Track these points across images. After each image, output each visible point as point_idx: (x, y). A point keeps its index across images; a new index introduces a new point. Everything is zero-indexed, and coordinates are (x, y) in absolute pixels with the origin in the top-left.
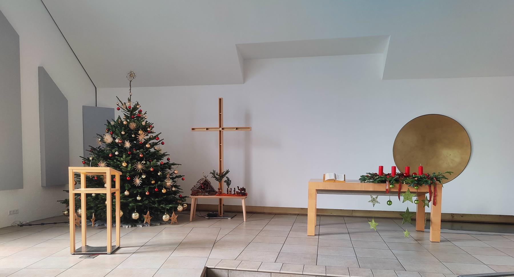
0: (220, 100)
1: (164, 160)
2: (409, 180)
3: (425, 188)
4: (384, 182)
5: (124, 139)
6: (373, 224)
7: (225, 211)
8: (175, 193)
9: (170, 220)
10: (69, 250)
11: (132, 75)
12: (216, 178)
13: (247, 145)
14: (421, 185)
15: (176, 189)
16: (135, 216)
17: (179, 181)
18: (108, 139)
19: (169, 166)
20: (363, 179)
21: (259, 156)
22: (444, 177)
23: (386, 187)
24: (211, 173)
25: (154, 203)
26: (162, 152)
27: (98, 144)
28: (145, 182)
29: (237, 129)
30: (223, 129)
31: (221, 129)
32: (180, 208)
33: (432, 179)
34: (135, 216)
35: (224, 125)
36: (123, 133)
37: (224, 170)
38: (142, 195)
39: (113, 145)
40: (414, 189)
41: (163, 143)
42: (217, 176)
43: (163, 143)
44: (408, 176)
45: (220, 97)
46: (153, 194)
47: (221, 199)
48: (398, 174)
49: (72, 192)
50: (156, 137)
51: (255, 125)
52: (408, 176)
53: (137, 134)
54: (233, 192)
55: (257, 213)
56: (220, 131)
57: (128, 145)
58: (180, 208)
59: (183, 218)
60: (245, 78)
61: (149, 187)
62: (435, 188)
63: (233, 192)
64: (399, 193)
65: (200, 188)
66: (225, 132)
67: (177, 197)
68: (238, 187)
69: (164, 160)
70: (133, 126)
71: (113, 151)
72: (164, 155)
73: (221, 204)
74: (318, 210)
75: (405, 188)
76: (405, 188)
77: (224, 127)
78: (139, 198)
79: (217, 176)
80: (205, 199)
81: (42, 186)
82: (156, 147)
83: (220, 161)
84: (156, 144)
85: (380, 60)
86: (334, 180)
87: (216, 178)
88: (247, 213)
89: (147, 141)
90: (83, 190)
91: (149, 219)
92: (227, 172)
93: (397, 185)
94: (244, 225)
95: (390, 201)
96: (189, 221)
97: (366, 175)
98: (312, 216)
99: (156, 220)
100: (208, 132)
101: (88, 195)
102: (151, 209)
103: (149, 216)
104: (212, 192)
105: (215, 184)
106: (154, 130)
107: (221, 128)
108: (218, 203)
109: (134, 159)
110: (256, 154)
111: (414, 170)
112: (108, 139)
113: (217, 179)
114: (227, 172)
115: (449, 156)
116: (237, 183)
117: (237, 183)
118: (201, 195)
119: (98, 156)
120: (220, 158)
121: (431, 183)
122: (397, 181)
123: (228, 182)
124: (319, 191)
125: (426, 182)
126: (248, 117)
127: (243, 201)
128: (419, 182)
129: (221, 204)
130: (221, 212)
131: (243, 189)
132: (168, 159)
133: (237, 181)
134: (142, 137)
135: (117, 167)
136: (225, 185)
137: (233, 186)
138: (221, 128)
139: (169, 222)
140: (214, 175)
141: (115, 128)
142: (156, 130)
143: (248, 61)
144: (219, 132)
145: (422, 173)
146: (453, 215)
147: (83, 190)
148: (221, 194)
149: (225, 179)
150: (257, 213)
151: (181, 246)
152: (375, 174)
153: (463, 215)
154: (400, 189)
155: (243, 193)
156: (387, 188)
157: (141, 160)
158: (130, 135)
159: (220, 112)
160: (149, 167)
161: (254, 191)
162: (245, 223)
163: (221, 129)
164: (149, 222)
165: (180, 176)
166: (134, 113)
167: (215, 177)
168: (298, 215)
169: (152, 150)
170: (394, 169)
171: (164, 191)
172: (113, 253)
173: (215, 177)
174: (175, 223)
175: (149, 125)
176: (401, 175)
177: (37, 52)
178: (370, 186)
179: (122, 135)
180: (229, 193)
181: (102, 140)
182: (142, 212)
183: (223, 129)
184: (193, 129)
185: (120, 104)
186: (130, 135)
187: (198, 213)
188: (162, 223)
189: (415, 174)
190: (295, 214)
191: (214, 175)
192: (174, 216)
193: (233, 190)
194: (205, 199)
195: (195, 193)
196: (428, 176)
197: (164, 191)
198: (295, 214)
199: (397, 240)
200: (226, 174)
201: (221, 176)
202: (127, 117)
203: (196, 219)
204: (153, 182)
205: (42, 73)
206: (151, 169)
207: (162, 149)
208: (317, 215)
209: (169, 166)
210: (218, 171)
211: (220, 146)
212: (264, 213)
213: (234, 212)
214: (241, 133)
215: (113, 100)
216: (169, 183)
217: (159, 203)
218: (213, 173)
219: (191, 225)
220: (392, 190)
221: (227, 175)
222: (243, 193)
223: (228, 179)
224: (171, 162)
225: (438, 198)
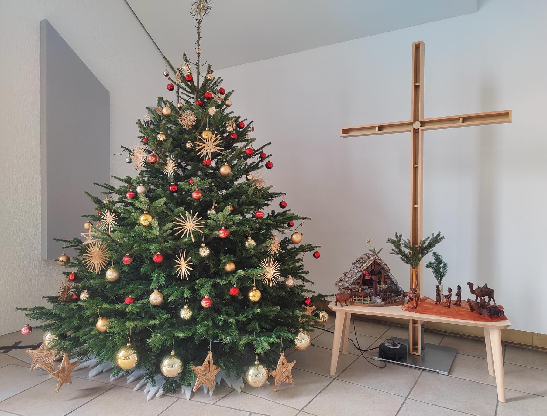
6: (419, 165)
12: (404, 255)
15: (299, 282)
16: (171, 366)
19: (284, 220)
24: (390, 241)
28: (201, 269)
31: (417, 125)
34: (171, 366)
35: (427, 114)
37: (426, 233)
42: (407, 251)
43: (269, 166)
56: (416, 131)
58: (302, 340)
60: (479, 8)
61: (215, 285)
65: (364, 281)
68: (471, 285)
69: (273, 207)
79: (407, 251)
82: (252, 175)
83: (415, 210)
84: (254, 167)
87: (404, 255)
92: (437, 240)
103: (213, 366)
104: (392, 295)
105: (400, 273)
106: (250, 135)
113: (407, 259)
114: (437, 240)
120: (415, 202)
123: (439, 269)
130: (415, 343)
136: (428, 279)
137: (450, 281)
140: (398, 247)
144: (410, 135)
149: (428, 258)
163: (417, 125)
165: (310, 248)
167: (401, 252)
183: (423, 124)
184: (345, 131)
191: (398, 247)
193: (455, 291)
204: (230, 267)
206: (222, 234)
207: (263, 178)
210: (408, 236)
211: (415, 169)
214: (472, 131)
218: (396, 243)
221: (436, 249)
223: (439, 260)
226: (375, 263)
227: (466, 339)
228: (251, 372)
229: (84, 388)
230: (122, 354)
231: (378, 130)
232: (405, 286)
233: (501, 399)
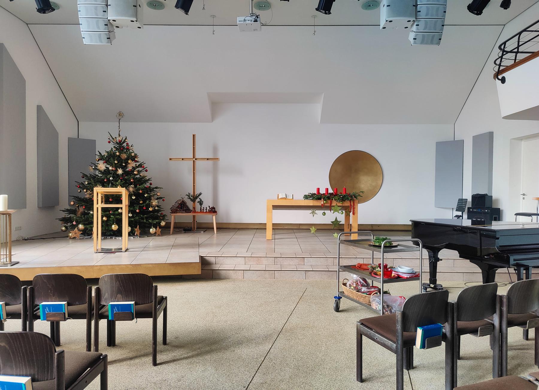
0: (194, 135)
1: (148, 185)
2: (337, 197)
3: (347, 204)
4: (319, 199)
7: (197, 228)
8: (158, 211)
9: (155, 233)
10: (93, 250)
13: (215, 172)
14: (344, 201)
18: (102, 166)
20: (306, 197)
21: (226, 183)
22: (359, 195)
23: (321, 203)
24: (187, 195)
25: (143, 219)
26: (147, 178)
27: (90, 171)
29: (208, 159)
30: (196, 159)
31: (194, 159)
32: (163, 223)
33: (351, 197)
36: (116, 162)
37: (197, 193)
39: (106, 172)
41: (146, 171)
43: (146, 171)
44: (336, 195)
46: (143, 212)
47: (194, 216)
48: (330, 194)
50: (140, 166)
51: (221, 156)
52: (336, 195)
53: (127, 163)
54: (205, 211)
55: (224, 228)
56: (194, 161)
57: (120, 172)
58: (163, 223)
59: (165, 231)
60: (213, 119)
62: (354, 203)
63: (205, 211)
64: (330, 208)
65: (178, 207)
66: (197, 162)
67: (159, 214)
69: (148, 185)
70: (124, 156)
71: (108, 176)
72: (149, 180)
73: (194, 221)
74: (273, 224)
75: (334, 203)
76: (334, 203)
77: (197, 157)
80: (185, 218)
81: (38, 207)
83: (194, 185)
84: (141, 171)
85: (317, 109)
86: (286, 198)
88: (217, 228)
89: (134, 168)
91: (139, 232)
92: (200, 194)
93: (329, 201)
94: (215, 235)
95: (324, 213)
96: (168, 234)
97: (308, 194)
98: (269, 228)
99: (145, 233)
100: (183, 161)
104: (188, 210)
105: (190, 204)
107: (195, 159)
108: (191, 220)
110: (224, 181)
111: (340, 191)
112: (102, 166)
113: (192, 200)
115: (365, 182)
116: (208, 203)
117: (208, 203)
118: (180, 213)
120: (194, 183)
121: (351, 200)
122: (329, 198)
123: (201, 203)
124: (275, 207)
125: (348, 198)
126: (215, 150)
127: (214, 217)
128: (343, 199)
129: (194, 221)
131: (213, 208)
132: (151, 184)
134: (131, 165)
137: (205, 205)
138: (195, 159)
139: (155, 234)
141: (109, 158)
142: (140, 159)
143: (217, 105)
145: (346, 193)
146: (372, 225)
148: (195, 212)
149: (198, 200)
150: (224, 228)
151: (174, 246)
152: (315, 194)
153: (379, 225)
154: (331, 204)
155: (213, 210)
156: (322, 203)
159: (194, 145)
160: (139, 189)
161: (221, 209)
162: (215, 235)
163: (194, 159)
164: (138, 234)
165: (161, 198)
166: (122, 146)
167: (190, 198)
168: (257, 229)
169: (138, 176)
170: (327, 190)
171: (150, 209)
172: (126, 251)
173: (190, 198)
174: (159, 235)
176: (331, 194)
177: (39, 92)
178: (311, 203)
179: (116, 164)
180: (201, 211)
181: (96, 169)
183: (196, 159)
184: (170, 159)
185: (111, 138)
187: (175, 230)
188: (149, 234)
189: (341, 193)
190: (255, 229)
192: (159, 230)
193: (205, 209)
194: (185, 218)
195: (174, 211)
196: (349, 195)
197: (150, 209)
198: (255, 229)
199: (328, 241)
200: (199, 196)
201: (194, 198)
203: (175, 233)
204: (141, 202)
205: (40, 109)
206: (141, 192)
207: (147, 175)
208: (273, 229)
210: (192, 193)
211: (194, 173)
212: (229, 229)
213: (206, 228)
214: (210, 162)
216: (155, 203)
219: (171, 236)
220: (326, 205)
222: (213, 210)
223: (201, 200)
224: (152, 186)
225: (355, 210)
226: (183, 201)
227: (239, 229)
228: (151, 230)
229: (38, 383)
230: (113, 226)
231: (102, 208)
232: (191, 208)
233: (196, 227)
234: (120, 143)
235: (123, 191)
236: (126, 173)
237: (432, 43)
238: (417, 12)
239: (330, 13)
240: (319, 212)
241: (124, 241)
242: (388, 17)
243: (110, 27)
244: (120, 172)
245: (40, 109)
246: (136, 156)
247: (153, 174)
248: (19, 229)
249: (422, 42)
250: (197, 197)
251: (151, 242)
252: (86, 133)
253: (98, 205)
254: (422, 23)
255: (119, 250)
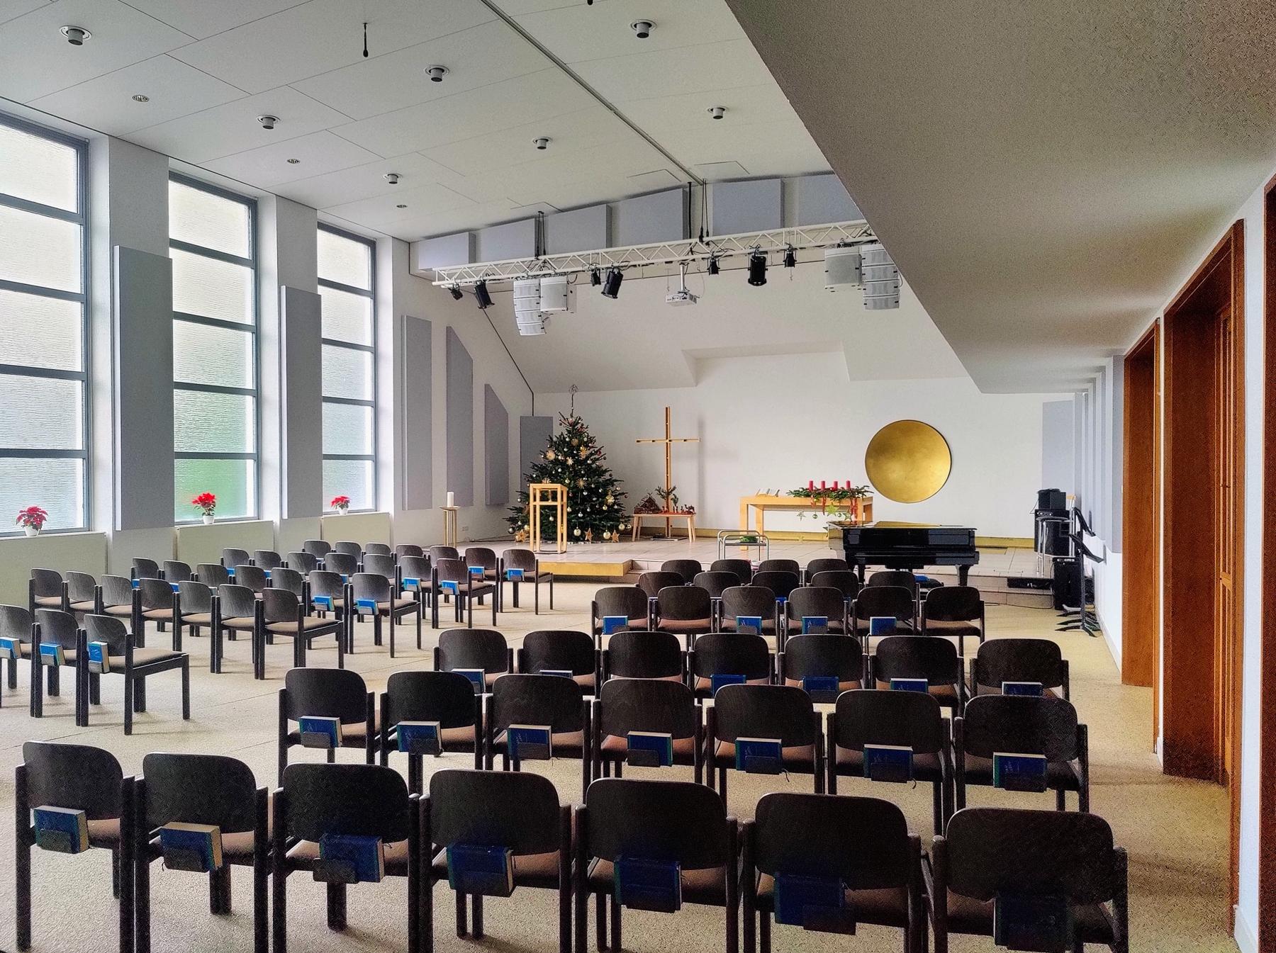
1: (607, 476)
3: (846, 502)
4: (808, 496)
5: (566, 455)
8: (617, 511)
11: (714, 269)
16: (577, 532)
17: (622, 499)
18: (551, 455)
19: (611, 482)
20: (797, 494)
23: (808, 501)
27: (540, 460)
34: (577, 532)
38: (584, 512)
40: (836, 503)
45: (609, 299)
49: (532, 503)
53: (578, 450)
58: (622, 527)
59: (626, 536)
60: (697, 384)
64: (823, 508)
65: (644, 506)
69: (607, 476)
70: (575, 442)
72: (606, 471)
75: (829, 502)
78: (580, 515)
80: (650, 520)
89: (587, 458)
90: (538, 503)
99: (598, 538)
101: (542, 507)
102: (593, 526)
104: (656, 510)
105: (660, 502)
109: (576, 475)
110: (711, 467)
112: (551, 455)
119: (544, 472)
126: (701, 426)
133: (687, 496)
134: (584, 453)
135: (562, 483)
136: (671, 503)
141: (559, 445)
142: (598, 445)
143: (700, 365)
147: (538, 503)
149: (671, 496)
157: (583, 476)
158: (572, 451)
166: (576, 429)
175: (591, 440)
182: (583, 529)
186: (572, 451)
188: (603, 540)
192: (616, 535)
194: (650, 520)
201: (667, 494)
202: (569, 432)
205: (488, 388)
209: (611, 482)
215: (557, 409)
216: (611, 500)
217: (601, 520)
222: (690, 511)
234: (573, 425)
235: (558, 487)
236: (577, 462)
237: (887, 307)
238: (861, 275)
239: (764, 282)
240: (809, 514)
241: (562, 544)
242: (250, 608)
243: (544, 318)
244: (570, 462)
245: (488, 388)
246: (591, 440)
247: (615, 460)
248: (466, 529)
249: (875, 308)
250: (668, 493)
251: (605, 547)
252: (541, 411)
253: (536, 504)
254: (869, 286)
255: (555, 552)
